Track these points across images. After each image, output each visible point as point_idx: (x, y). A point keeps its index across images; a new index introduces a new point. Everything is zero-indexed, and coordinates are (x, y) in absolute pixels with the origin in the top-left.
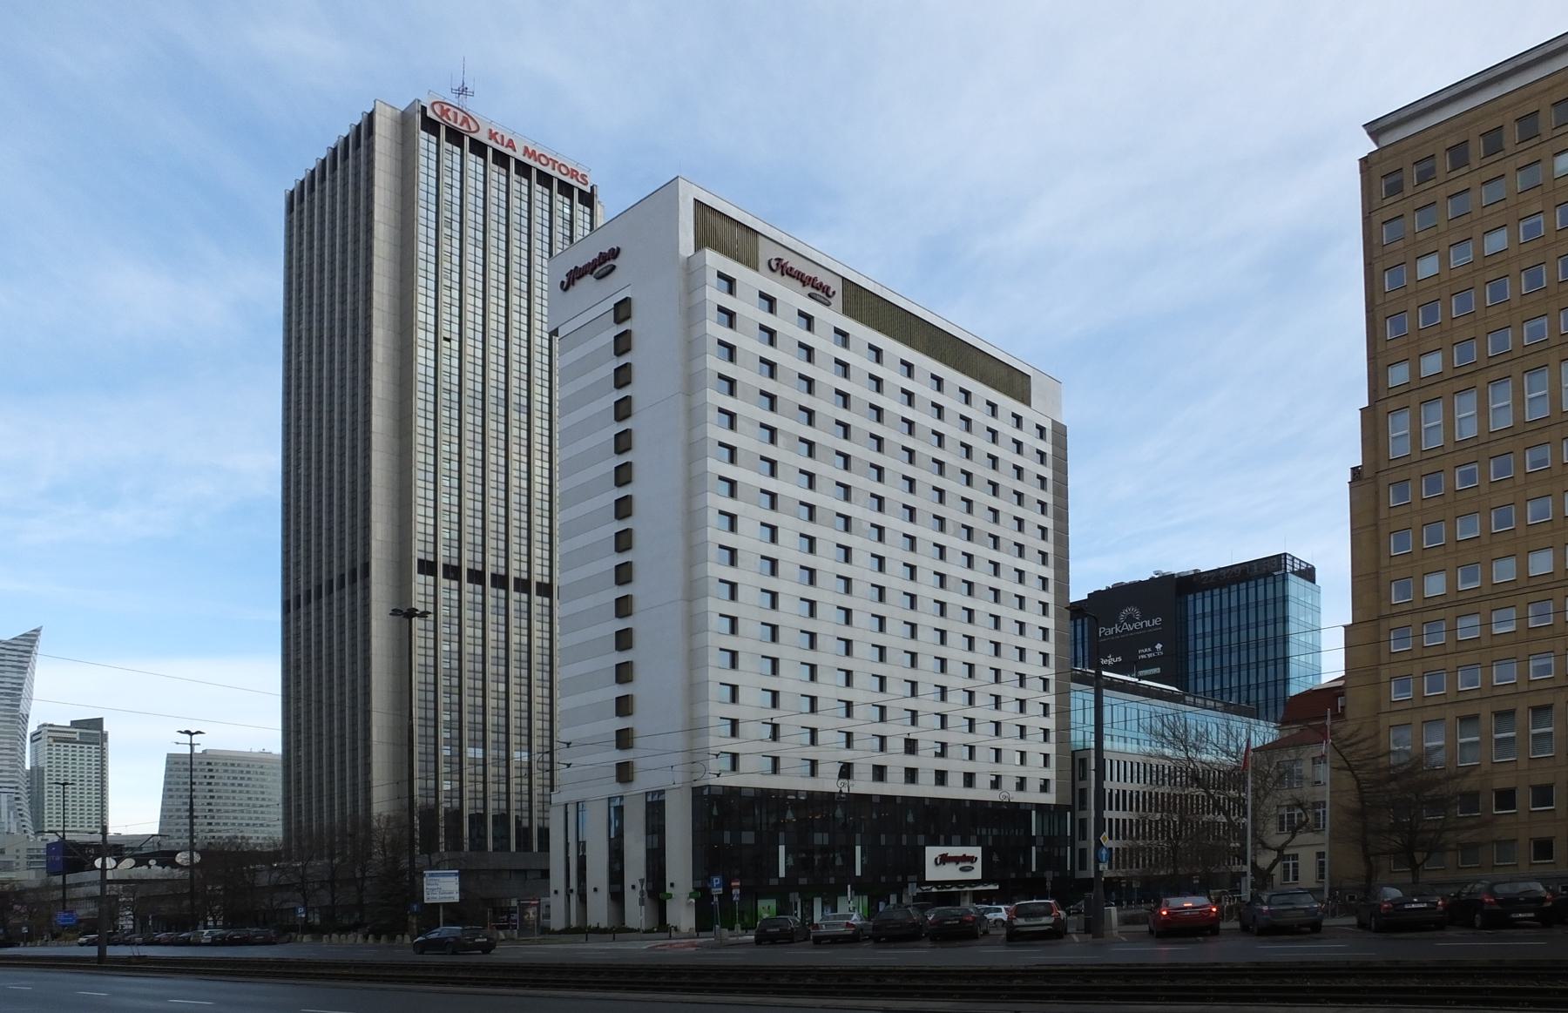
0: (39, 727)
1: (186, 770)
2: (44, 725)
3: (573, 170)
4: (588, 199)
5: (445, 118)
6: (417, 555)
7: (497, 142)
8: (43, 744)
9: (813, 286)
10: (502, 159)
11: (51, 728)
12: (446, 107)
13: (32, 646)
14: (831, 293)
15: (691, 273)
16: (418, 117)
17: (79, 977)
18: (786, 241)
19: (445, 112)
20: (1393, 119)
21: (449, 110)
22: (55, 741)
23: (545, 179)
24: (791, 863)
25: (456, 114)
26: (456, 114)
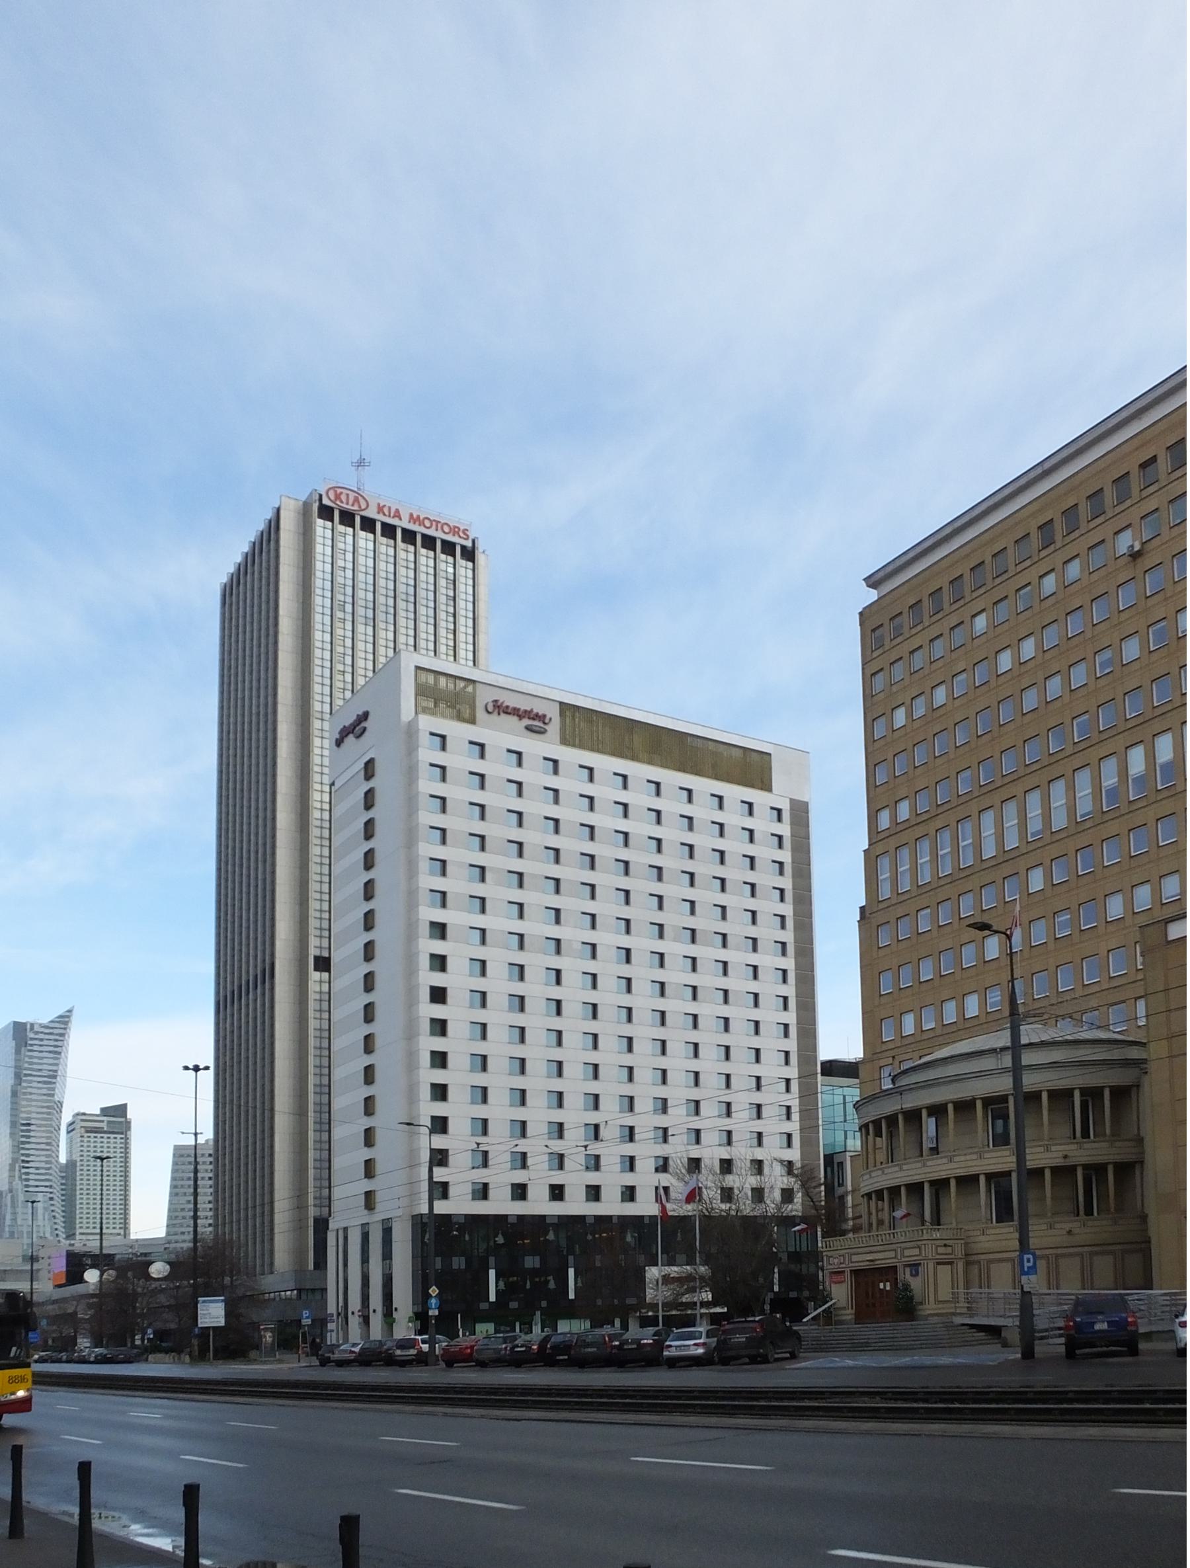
0: (74, 1116)
1: (190, 1163)
2: (78, 1114)
3: (455, 527)
4: (470, 554)
5: (338, 502)
6: (313, 952)
7: (384, 515)
8: (79, 1131)
9: (529, 718)
10: (389, 531)
11: (84, 1117)
12: (339, 491)
13: (65, 1029)
14: (547, 721)
15: (411, 731)
16: (316, 506)
17: (105, 1397)
18: (502, 682)
19: (338, 496)
20: (881, 574)
21: (341, 493)
22: (87, 1132)
23: (429, 542)
24: (502, 1285)
25: (348, 495)
26: (348, 495)
